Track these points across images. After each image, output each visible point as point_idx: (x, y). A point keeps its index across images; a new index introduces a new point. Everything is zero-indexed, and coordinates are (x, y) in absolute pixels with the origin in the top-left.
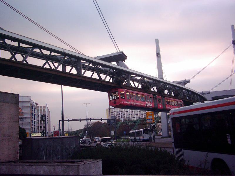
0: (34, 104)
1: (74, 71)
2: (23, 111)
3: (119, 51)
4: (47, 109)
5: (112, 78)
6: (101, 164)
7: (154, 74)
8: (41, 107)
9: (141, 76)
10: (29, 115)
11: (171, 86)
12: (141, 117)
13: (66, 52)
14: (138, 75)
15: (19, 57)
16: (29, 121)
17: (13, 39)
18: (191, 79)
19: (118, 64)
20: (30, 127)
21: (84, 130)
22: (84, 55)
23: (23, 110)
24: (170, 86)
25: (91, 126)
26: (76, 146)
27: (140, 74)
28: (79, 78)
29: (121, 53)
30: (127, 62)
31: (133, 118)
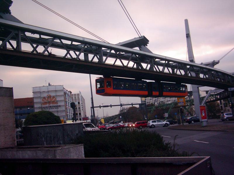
0: (67, 92)
1: (96, 60)
2: (57, 100)
3: (140, 36)
4: (82, 96)
5: (135, 64)
6: (83, 149)
7: (182, 56)
8: (75, 95)
9: (165, 60)
10: (63, 104)
11: (199, 68)
12: (149, 102)
13: (86, 40)
14: (162, 59)
15: (41, 49)
16: (64, 108)
17: (34, 32)
18: (221, 59)
19: (141, 49)
20: (65, 115)
21: (119, 115)
22: (109, 43)
23: (57, 99)
24: (197, 69)
25: (126, 111)
26: (79, 132)
27: (164, 58)
28: (100, 66)
29: (143, 38)
30: (149, 47)
31: (168, 101)
